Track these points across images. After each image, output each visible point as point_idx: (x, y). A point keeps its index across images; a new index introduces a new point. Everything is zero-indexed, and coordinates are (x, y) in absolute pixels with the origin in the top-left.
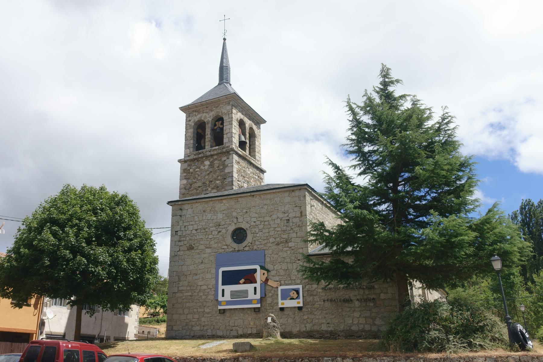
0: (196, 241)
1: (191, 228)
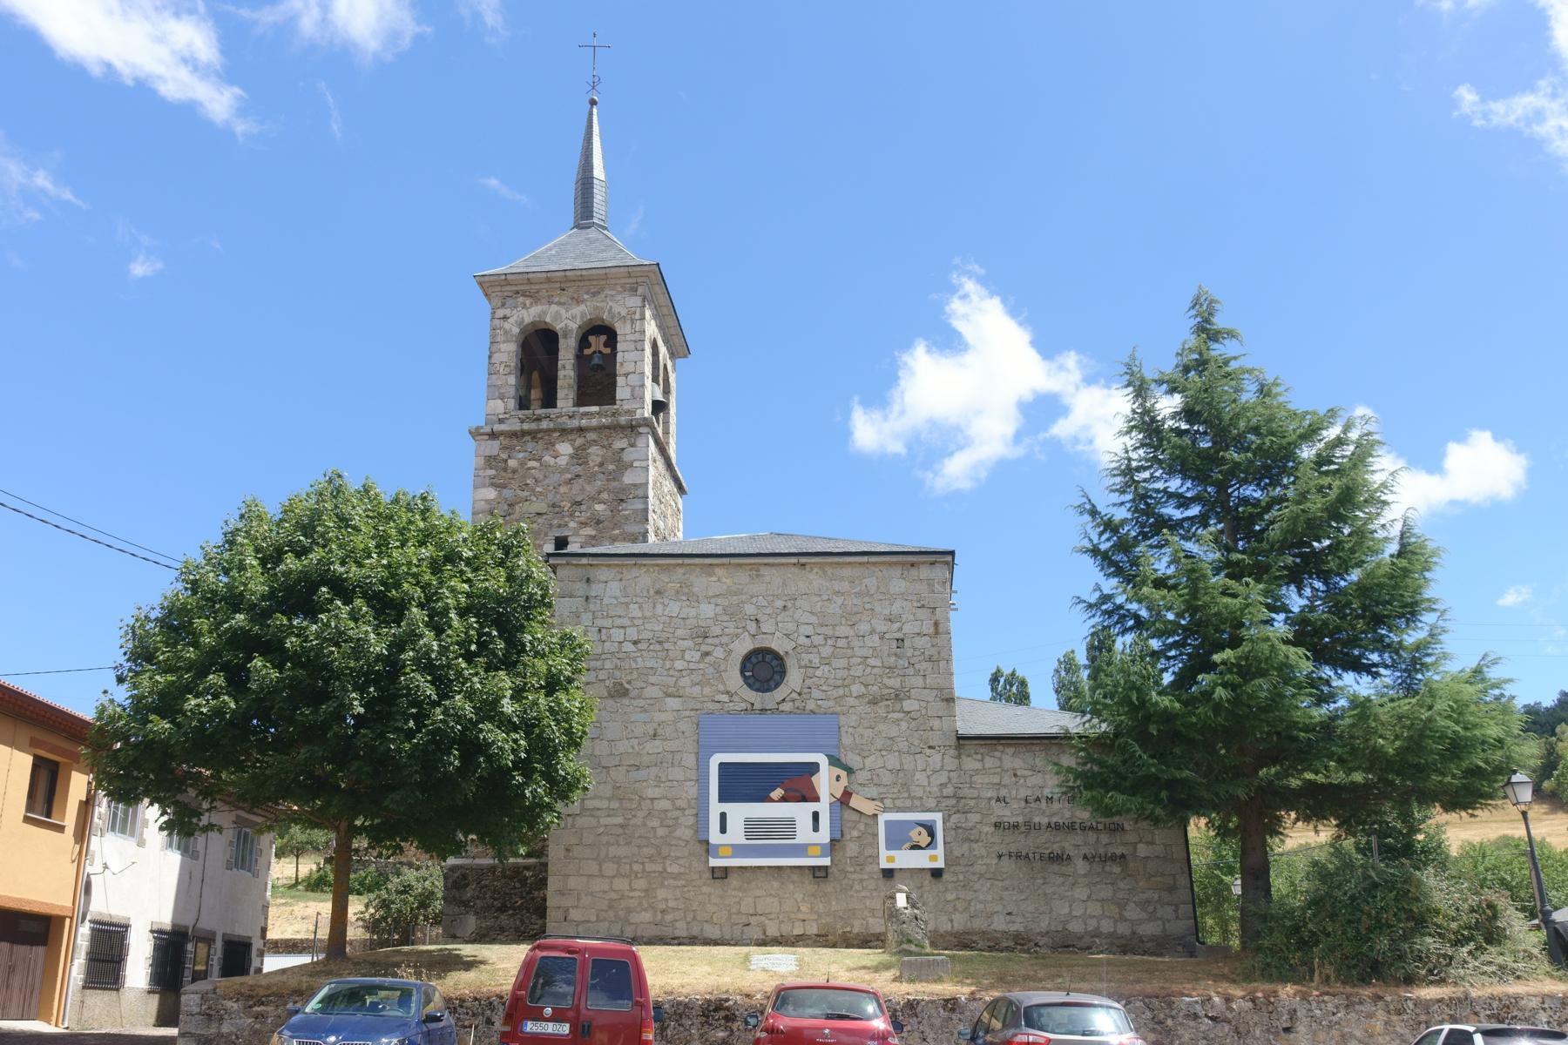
0: (635, 675)
1: (617, 634)
